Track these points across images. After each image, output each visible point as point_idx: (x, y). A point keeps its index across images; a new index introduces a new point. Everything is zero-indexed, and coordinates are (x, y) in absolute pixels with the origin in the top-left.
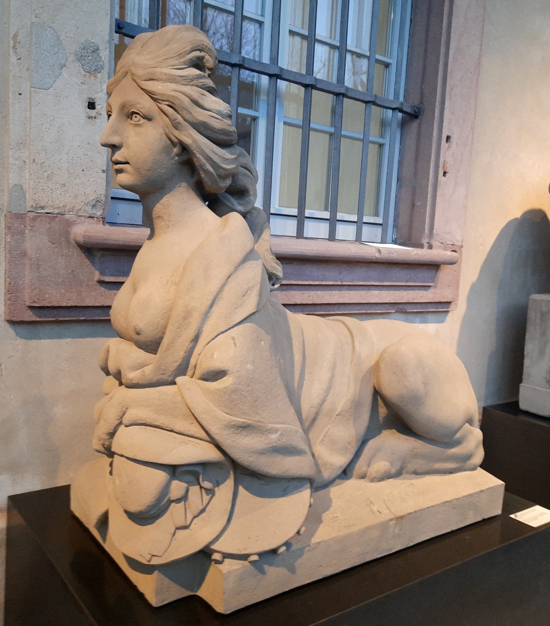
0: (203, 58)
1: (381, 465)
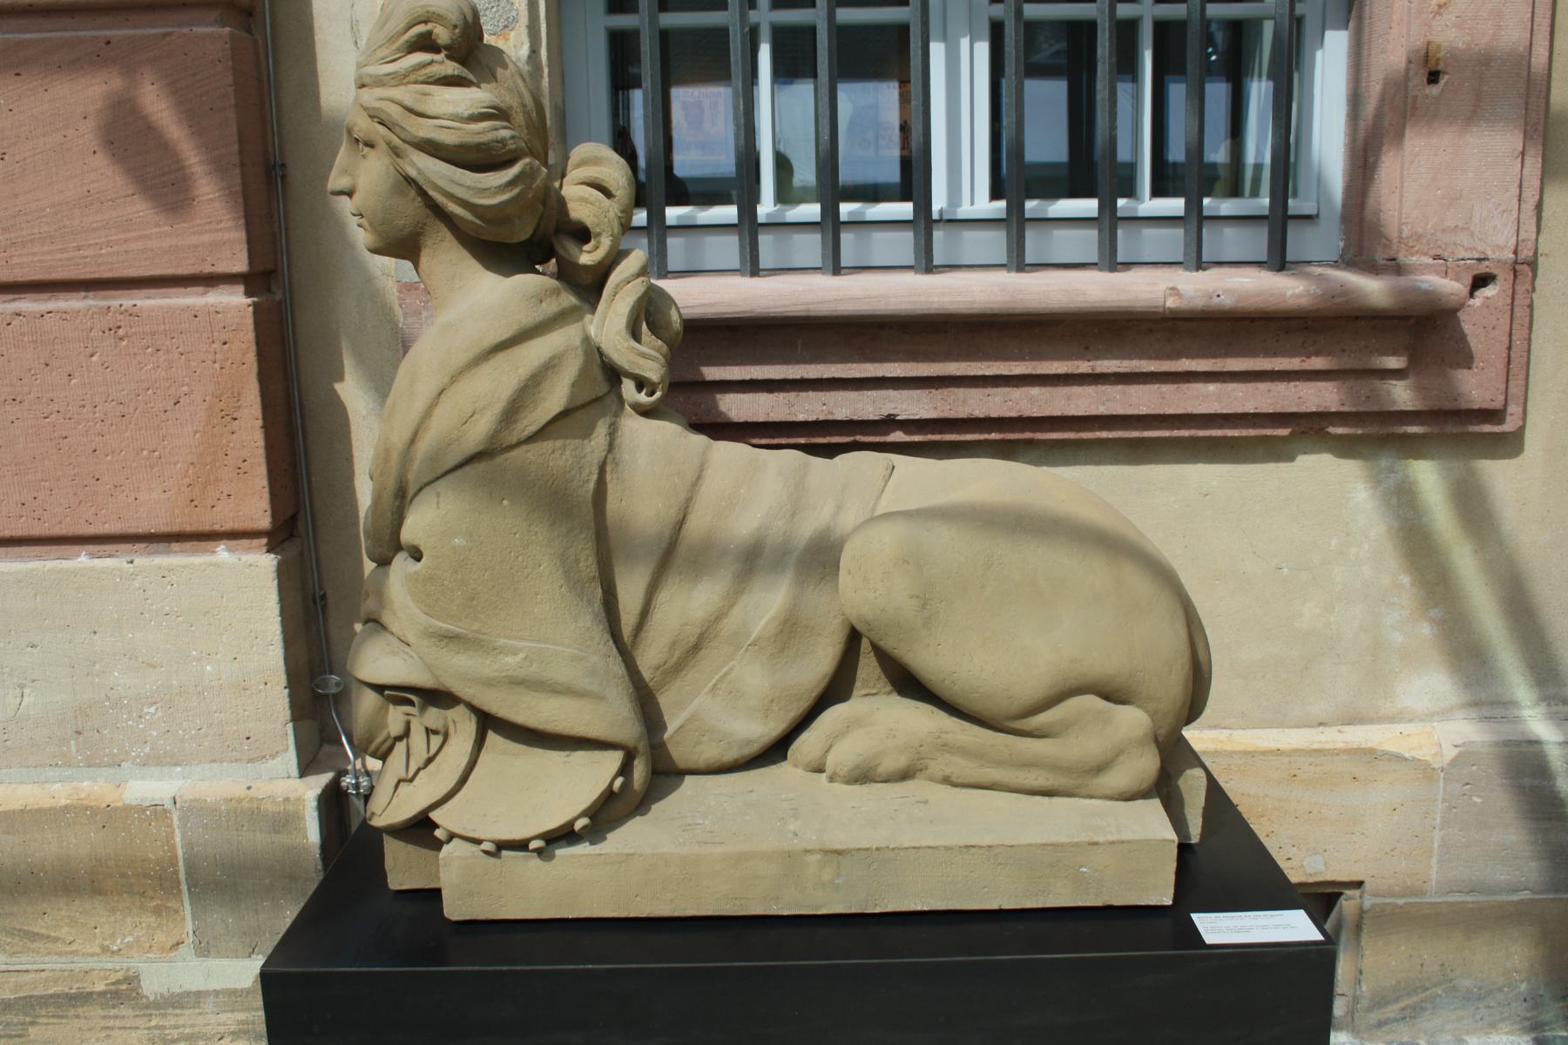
0: (430, 33)
1: (845, 755)
